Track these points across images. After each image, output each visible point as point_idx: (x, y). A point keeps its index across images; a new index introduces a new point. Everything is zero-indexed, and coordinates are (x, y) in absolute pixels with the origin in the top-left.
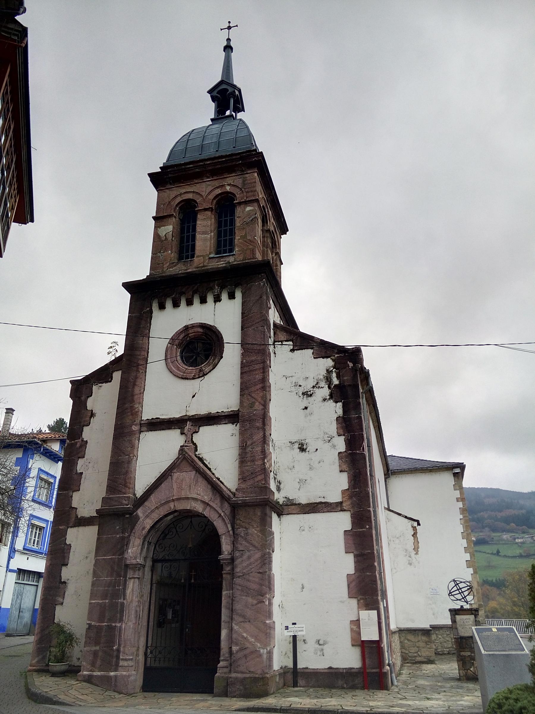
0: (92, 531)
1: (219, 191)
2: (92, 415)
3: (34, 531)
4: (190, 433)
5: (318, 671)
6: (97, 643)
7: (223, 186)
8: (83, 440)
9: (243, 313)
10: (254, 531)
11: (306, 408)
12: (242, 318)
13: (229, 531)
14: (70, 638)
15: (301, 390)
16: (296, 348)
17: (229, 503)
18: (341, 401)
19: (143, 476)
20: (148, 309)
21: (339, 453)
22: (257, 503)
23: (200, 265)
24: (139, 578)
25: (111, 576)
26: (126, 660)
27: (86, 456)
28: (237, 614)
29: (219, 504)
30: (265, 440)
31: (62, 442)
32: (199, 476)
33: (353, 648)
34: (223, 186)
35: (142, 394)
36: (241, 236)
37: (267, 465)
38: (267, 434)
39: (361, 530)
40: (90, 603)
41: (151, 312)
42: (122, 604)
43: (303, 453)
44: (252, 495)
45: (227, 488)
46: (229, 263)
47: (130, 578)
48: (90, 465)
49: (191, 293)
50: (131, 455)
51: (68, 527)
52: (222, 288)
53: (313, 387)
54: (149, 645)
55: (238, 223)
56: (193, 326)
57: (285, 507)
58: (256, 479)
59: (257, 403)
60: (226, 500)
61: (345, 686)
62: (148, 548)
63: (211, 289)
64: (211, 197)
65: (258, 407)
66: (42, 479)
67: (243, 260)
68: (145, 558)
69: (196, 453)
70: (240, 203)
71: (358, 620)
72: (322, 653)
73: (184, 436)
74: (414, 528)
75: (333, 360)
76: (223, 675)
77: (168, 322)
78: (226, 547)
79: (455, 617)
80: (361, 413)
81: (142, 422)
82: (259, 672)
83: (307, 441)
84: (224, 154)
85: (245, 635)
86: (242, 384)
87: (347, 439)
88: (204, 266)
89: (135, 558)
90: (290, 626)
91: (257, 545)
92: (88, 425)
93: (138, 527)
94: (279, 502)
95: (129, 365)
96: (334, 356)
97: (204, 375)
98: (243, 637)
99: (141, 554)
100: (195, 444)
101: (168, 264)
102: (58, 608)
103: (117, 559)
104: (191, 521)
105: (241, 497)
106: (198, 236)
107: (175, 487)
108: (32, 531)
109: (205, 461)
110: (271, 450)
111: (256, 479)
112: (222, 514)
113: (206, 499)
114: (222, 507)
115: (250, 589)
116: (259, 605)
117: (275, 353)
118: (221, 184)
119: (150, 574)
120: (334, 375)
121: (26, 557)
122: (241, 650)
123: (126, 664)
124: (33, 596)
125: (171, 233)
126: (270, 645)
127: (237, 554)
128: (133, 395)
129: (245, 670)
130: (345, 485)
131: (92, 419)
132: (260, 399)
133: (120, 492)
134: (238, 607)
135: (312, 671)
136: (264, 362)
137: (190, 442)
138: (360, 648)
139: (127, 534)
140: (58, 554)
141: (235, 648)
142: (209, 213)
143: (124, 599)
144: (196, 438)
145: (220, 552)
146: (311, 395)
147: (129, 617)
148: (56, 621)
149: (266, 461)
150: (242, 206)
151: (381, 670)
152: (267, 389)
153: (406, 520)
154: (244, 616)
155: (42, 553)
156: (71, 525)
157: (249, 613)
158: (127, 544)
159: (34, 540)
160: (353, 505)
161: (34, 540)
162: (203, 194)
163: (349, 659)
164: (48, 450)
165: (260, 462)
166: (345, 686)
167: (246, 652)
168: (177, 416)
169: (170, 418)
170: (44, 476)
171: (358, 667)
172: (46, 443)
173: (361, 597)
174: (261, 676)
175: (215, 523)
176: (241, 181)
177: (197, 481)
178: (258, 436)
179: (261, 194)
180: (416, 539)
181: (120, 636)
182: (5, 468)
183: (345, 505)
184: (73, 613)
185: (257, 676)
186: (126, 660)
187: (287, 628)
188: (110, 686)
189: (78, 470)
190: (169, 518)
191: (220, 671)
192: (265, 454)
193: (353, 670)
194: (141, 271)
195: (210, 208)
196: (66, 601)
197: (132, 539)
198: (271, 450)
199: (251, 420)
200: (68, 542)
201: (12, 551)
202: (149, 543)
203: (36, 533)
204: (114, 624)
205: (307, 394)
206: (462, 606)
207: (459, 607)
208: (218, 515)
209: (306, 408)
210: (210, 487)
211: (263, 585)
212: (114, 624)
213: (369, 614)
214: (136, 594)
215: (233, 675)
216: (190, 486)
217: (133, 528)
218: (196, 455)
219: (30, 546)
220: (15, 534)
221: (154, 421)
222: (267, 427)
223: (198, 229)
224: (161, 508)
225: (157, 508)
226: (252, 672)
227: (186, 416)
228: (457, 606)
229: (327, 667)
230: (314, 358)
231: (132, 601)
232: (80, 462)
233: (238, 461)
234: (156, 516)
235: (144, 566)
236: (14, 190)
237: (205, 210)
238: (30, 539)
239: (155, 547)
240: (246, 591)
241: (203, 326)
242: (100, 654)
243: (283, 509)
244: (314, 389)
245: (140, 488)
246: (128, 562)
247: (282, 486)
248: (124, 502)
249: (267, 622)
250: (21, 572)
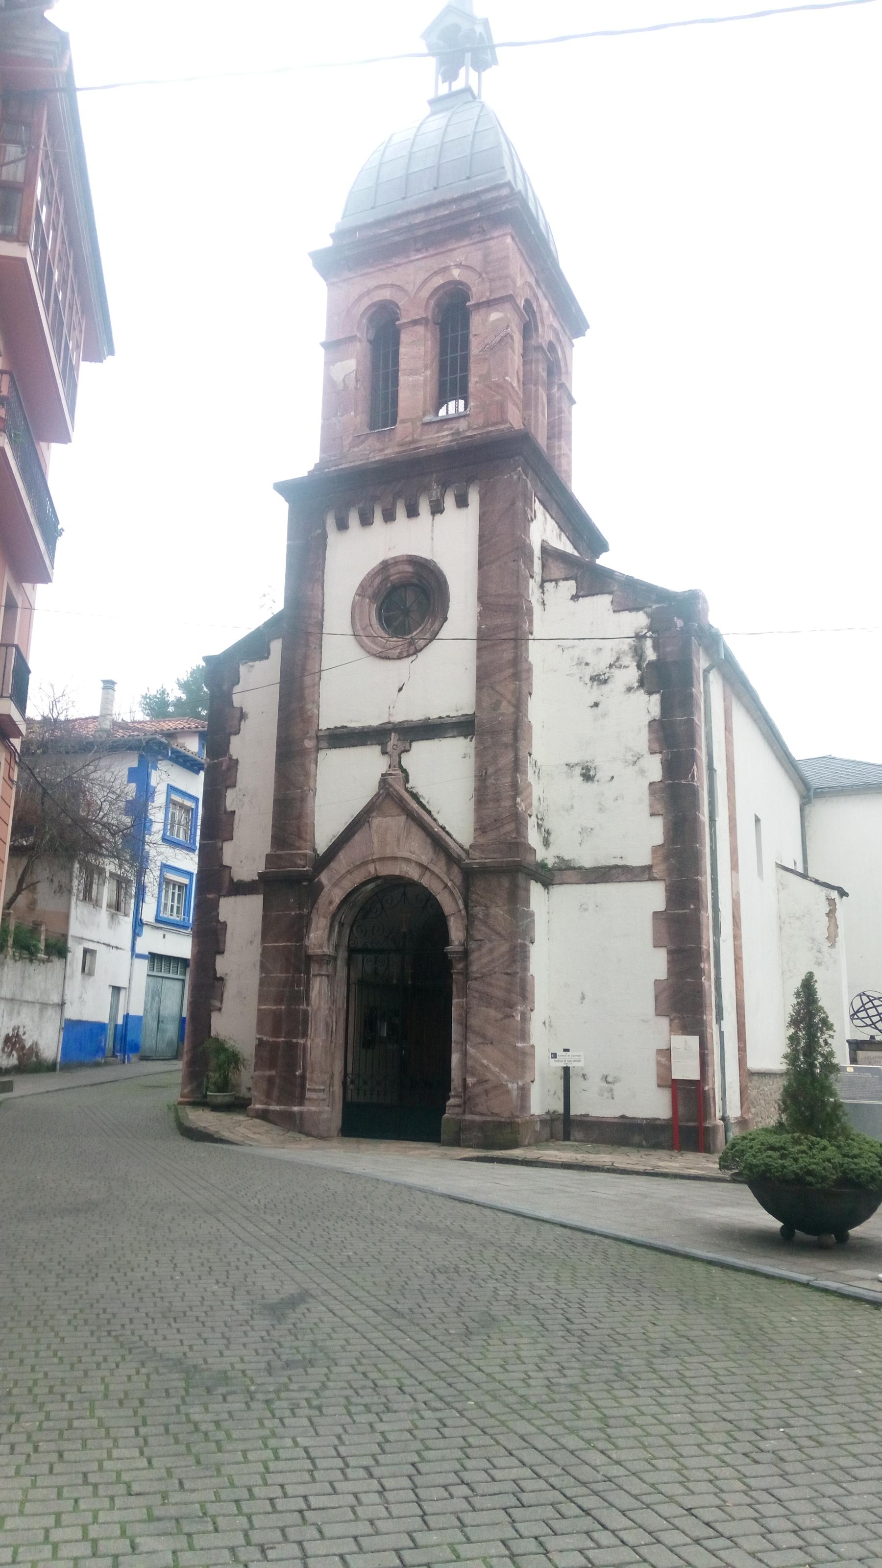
0: (254, 904)
1: (439, 281)
2: (243, 716)
3: (171, 891)
4: (396, 753)
5: (604, 1120)
6: (272, 1065)
7: (446, 269)
8: (230, 759)
9: (481, 537)
10: (498, 911)
11: (596, 705)
12: (481, 544)
13: (460, 911)
14: (234, 1059)
15: (589, 672)
16: (582, 593)
17: (460, 868)
18: (658, 692)
19: (327, 821)
20: (319, 531)
21: (651, 784)
22: (504, 869)
23: (408, 439)
24: (328, 976)
25: (287, 971)
26: (315, 1090)
27: (238, 787)
28: (474, 1032)
29: (444, 869)
30: (517, 766)
31: (202, 736)
32: (412, 823)
33: (660, 1090)
34: (446, 269)
35: (316, 688)
36: (480, 376)
37: (522, 807)
38: (522, 754)
39: (681, 912)
40: (259, 1010)
41: (324, 536)
42: (306, 1013)
43: (589, 784)
44: (495, 856)
45: (457, 843)
46: (458, 433)
47: (315, 976)
48: (246, 799)
49: (390, 498)
50: (305, 788)
51: (220, 896)
52: (445, 486)
53: (611, 666)
54: (350, 1070)
55: (475, 348)
56: (396, 561)
57: (556, 873)
58: (503, 831)
59: (504, 703)
60: (455, 862)
61: (644, 1143)
62: (340, 933)
63: (426, 488)
64: (425, 293)
65: (506, 708)
66: (175, 803)
67: (484, 427)
68: (337, 947)
69: (408, 786)
70: (478, 306)
71: (669, 1050)
72: (610, 1095)
73: (386, 757)
74: (831, 902)
75: (649, 615)
76: (454, 1116)
77: (359, 552)
78: (456, 933)
79: (856, 1054)
80: (692, 714)
81: (320, 734)
82: (507, 1114)
83: (596, 764)
84: (448, 196)
85: (485, 1062)
86: (479, 668)
87: (666, 760)
88: (414, 441)
89: (321, 946)
90: (560, 1053)
91: (503, 932)
92: (237, 732)
93: (322, 900)
94: (546, 865)
95: (295, 633)
96: (651, 607)
97: (417, 651)
98: (482, 1065)
99: (329, 940)
100: (404, 771)
101: (351, 438)
102: (215, 1016)
103: (293, 949)
104: (405, 892)
105: (477, 859)
106: (402, 379)
107: (375, 839)
108: (167, 892)
109: (421, 800)
110: (530, 780)
111: (503, 831)
112: (449, 884)
113: (424, 860)
114: (448, 872)
115: (492, 997)
116: (506, 1021)
117: (543, 603)
118: (443, 266)
119: (345, 969)
120: (649, 643)
121: (161, 933)
122: (481, 1082)
123: (315, 1097)
124: (175, 998)
125: (353, 375)
126: (522, 1077)
127: (473, 945)
128: (302, 689)
129: (485, 1111)
130: (658, 838)
131: (242, 723)
132: (509, 696)
133: (291, 846)
134: (474, 1022)
135: (594, 1119)
136: (516, 628)
137: (397, 766)
138: (670, 1089)
139: (306, 911)
140: (210, 936)
141: (470, 1080)
142: (420, 329)
143: (308, 1005)
144: (407, 761)
145: (445, 939)
146: (605, 682)
147: (316, 1029)
148: (213, 1034)
149: (518, 800)
150: (483, 311)
151: (701, 1123)
152: (524, 676)
153: (817, 887)
154: (484, 1036)
155: (186, 928)
156: (224, 892)
157: (491, 1031)
158: (308, 925)
159: (172, 906)
160: (670, 871)
161: (172, 906)
162: (410, 288)
163: (655, 1105)
164: (179, 752)
165: (507, 803)
166: (644, 1143)
167: (487, 1086)
168: (375, 722)
169: (363, 728)
170: (175, 797)
171: (665, 1117)
172: (176, 738)
173: (675, 1015)
174: (508, 1121)
175: (438, 897)
176: (479, 255)
177: (409, 833)
178: (506, 759)
179: (522, 275)
180: (833, 920)
181: (304, 1057)
182: (113, 792)
183: (657, 871)
184: (237, 1022)
185: (503, 1120)
186: (315, 1090)
187: (554, 1056)
188: (295, 1125)
189: (227, 806)
190: (370, 887)
191: (450, 1111)
192: (516, 789)
193: (658, 1122)
194: (303, 457)
195: (422, 318)
196: (225, 1006)
197: (315, 918)
198: (531, 777)
199: (494, 732)
200: (222, 918)
201: (138, 925)
202: (342, 925)
203: (173, 894)
204: (294, 1040)
205: (599, 680)
206: (872, 1037)
207: (868, 1038)
208: (442, 886)
209: (596, 705)
210: (429, 841)
211: (517, 990)
212: (294, 1040)
213: (686, 1041)
214: (324, 997)
215: (468, 1117)
216: (399, 839)
217: (314, 902)
218: (406, 789)
219: (166, 916)
220: (140, 896)
221: (337, 731)
222: (522, 744)
223: (403, 364)
224: (356, 872)
225: (349, 872)
226: (497, 1115)
227: (389, 723)
228: (864, 1034)
229: (617, 1115)
230: (614, 611)
231: (319, 1008)
232: (230, 794)
233: (473, 800)
234: (348, 885)
235: (335, 959)
236: (77, 312)
237: (415, 322)
238: (166, 905)
239: (351, 930)
240: (487, 999)
241: (414, 561)
242: (278, 1081)
243: (553, 875)
244: (612, 670)
245: (323, 839)
246: (310, 952)
247: (552, 839)
248: (299, 862)
249: (519, 1045)
250: (155, 959)
